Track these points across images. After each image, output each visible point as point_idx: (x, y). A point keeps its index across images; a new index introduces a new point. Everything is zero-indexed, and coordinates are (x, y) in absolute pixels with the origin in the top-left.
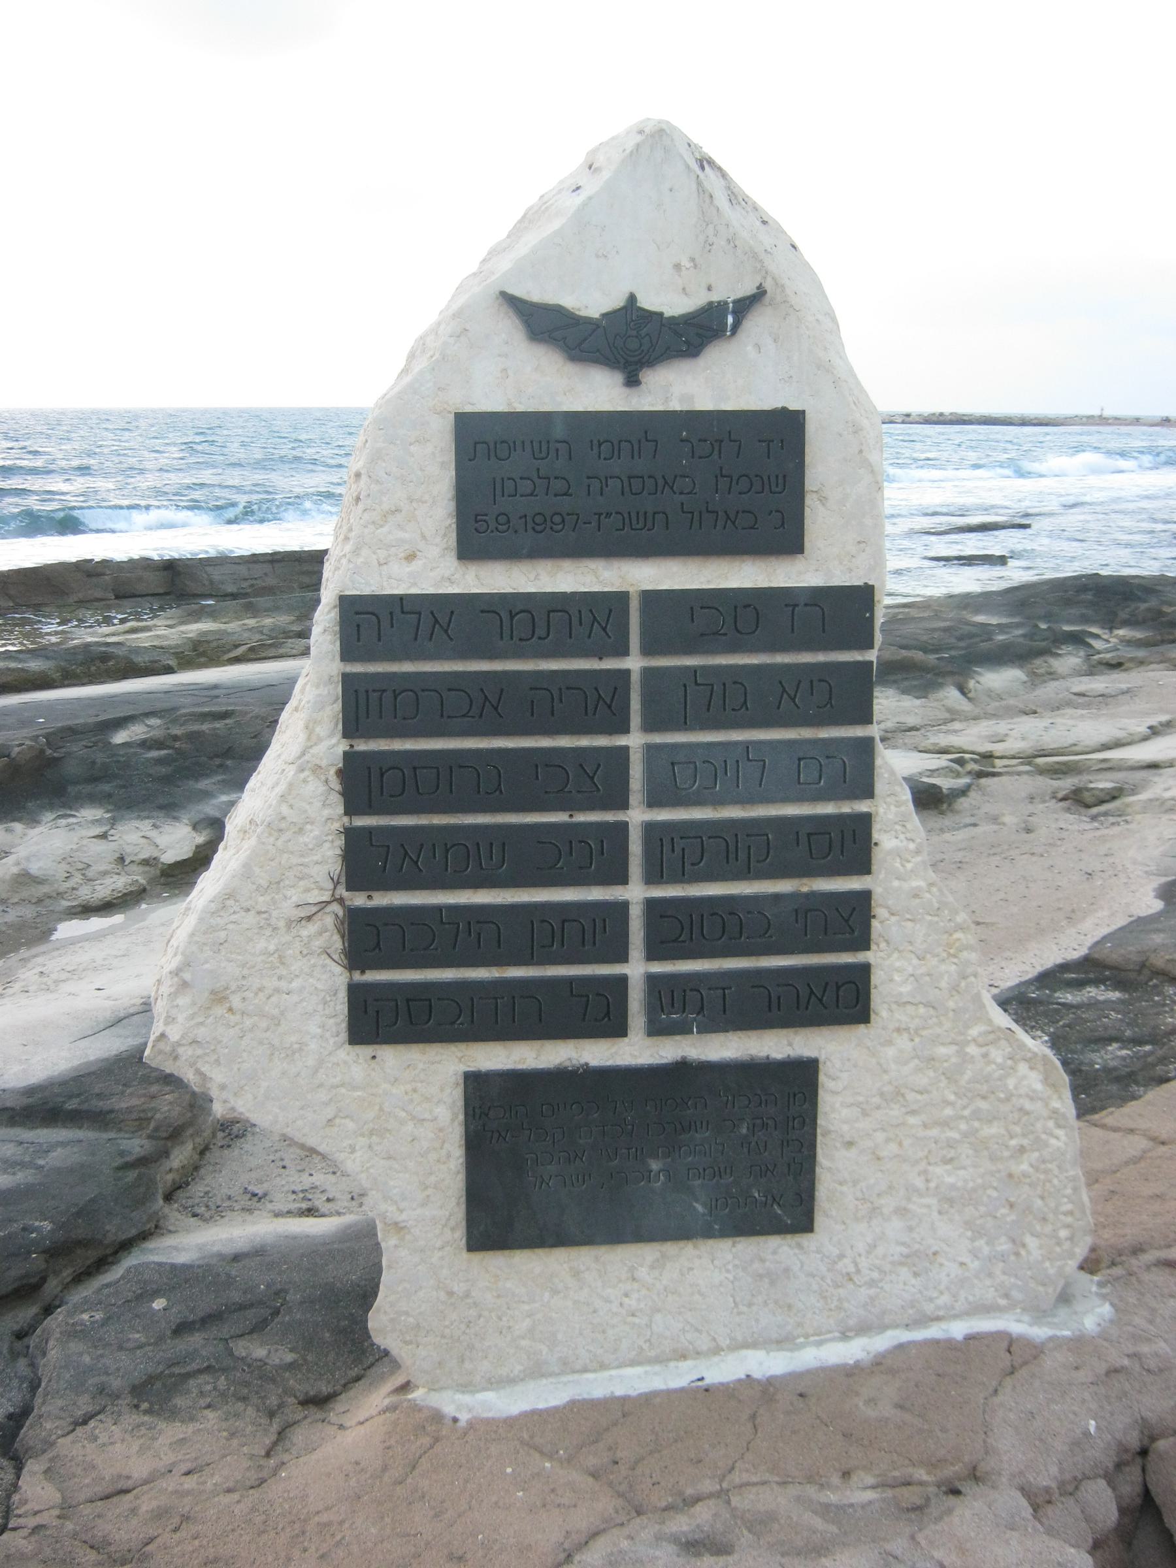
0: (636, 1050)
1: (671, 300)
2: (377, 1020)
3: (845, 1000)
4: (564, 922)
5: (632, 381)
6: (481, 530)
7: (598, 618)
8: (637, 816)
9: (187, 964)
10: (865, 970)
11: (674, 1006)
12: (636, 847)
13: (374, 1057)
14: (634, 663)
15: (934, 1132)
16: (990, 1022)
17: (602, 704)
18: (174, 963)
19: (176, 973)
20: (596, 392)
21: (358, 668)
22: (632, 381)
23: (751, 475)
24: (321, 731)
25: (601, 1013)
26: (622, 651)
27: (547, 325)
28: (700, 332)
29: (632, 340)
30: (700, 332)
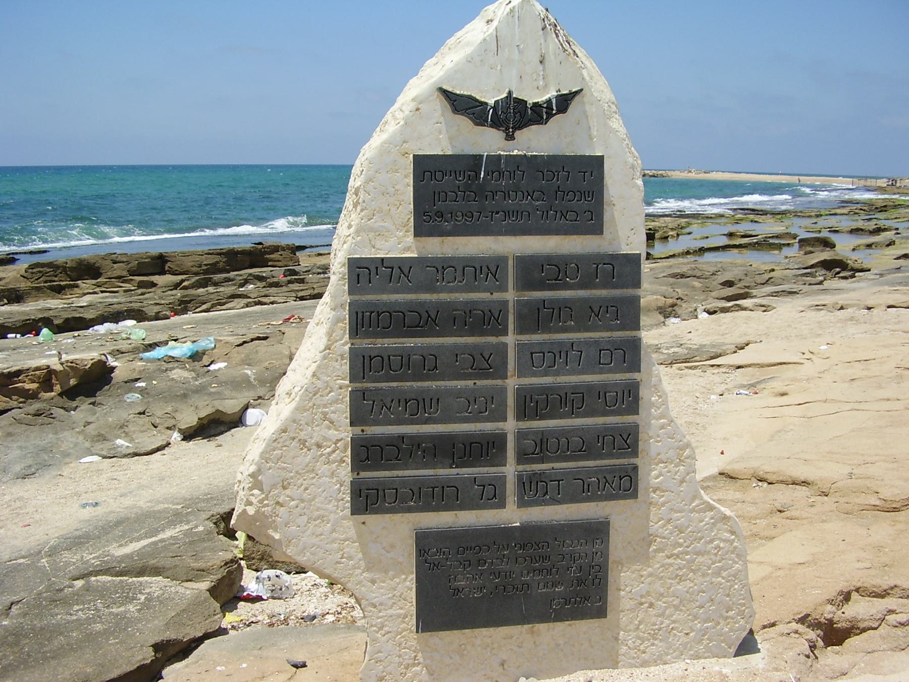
0: (512, 515)
1: (533, 97)
2: (366, 500)
3: (625, 484)
4: (532, 354)
5: (510, 137)
6: (429, 217)
7: (488, 270)
8: (512, 383)
9: (259, 471)
10: (635, 468)
11: (534, 489)
12: (511, 401)
13: (364, 523)
14: (510, 296)
15: (671, 561)
16: (702, 499)
17: (489, 320)
18: (253, 469)
19: (252, 475)
20: (489, 142)
21: (357, 297)
22: (510, 137)
23: (573, 190)
24: (338, 332)
25: (491, 495)
26: (503, 288)
27: (461, 105)
28: (539, 114)
29: (515, 115)
30: (539, 114)
